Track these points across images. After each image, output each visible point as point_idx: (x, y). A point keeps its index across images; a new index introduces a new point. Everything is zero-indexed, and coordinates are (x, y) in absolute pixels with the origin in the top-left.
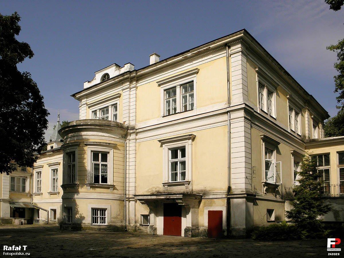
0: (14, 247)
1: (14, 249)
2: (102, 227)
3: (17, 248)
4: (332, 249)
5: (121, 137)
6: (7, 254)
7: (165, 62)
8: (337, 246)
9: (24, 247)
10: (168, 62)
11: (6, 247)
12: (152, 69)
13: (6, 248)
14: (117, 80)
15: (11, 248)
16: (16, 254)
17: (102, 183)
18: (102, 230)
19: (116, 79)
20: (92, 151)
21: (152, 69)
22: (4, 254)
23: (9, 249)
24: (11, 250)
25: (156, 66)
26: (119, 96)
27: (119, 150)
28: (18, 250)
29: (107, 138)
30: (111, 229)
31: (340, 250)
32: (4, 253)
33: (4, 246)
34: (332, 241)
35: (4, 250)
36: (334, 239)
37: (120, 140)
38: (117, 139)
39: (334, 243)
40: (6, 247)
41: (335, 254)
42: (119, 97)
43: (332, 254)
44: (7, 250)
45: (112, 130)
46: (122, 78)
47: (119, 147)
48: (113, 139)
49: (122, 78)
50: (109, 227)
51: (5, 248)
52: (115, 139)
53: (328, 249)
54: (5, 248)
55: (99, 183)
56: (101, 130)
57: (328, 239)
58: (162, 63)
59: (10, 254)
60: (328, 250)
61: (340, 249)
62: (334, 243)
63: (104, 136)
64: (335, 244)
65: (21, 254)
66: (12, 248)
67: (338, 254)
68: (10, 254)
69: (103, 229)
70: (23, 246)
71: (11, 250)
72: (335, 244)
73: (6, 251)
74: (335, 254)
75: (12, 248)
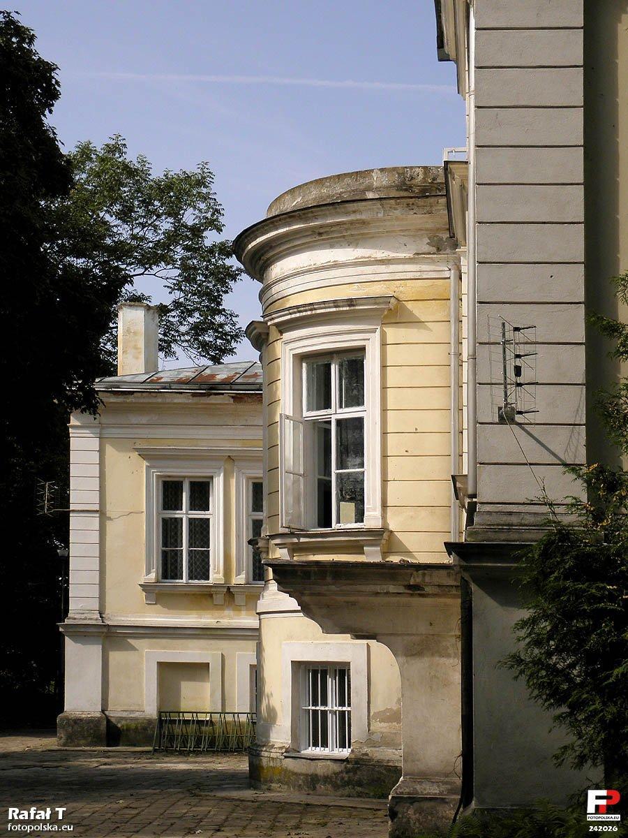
0: (35, 812)
2: (320, 769)
3: (42, 813)
4: (598, 816)
5: (426, 248)
8: (610, 809)
9: (58, 811)
11: (14, 811)
15: (26, 813)
16: (40, 828)
18: (321, 787)
22: (11, 828)
24: (27, 818)
27: (415, 322)
28: (43, 818)
29: (351, 271)
30: (360, 784)
31: (619, 820)
32: (9, 826)
33: (11, 810)
34: (598, 798)
35: (10, 818)
36: (603, 793)
37: (424, 267)
38: (400, 267)
39: (603, 802)
40: (14, 811)
43: (599, 828)
44: (16, 818)
45: (363, 222)
47: (416, 309)
48: (382, 268)
50: (354, 771)
52: (393, 268)
54: (13, 813)
56: (320, 234)
59: (24, 828)
60: (590, 820)
61: (619, 816)
62: (603, 802)
63: (336, 265)
64: (605, 804)
68: (24, 828)
69: (326, 779)
70: (57, 809)
71: (27, 818)
72: (605, 804)
73: (14, 821)
74: (605, 829)
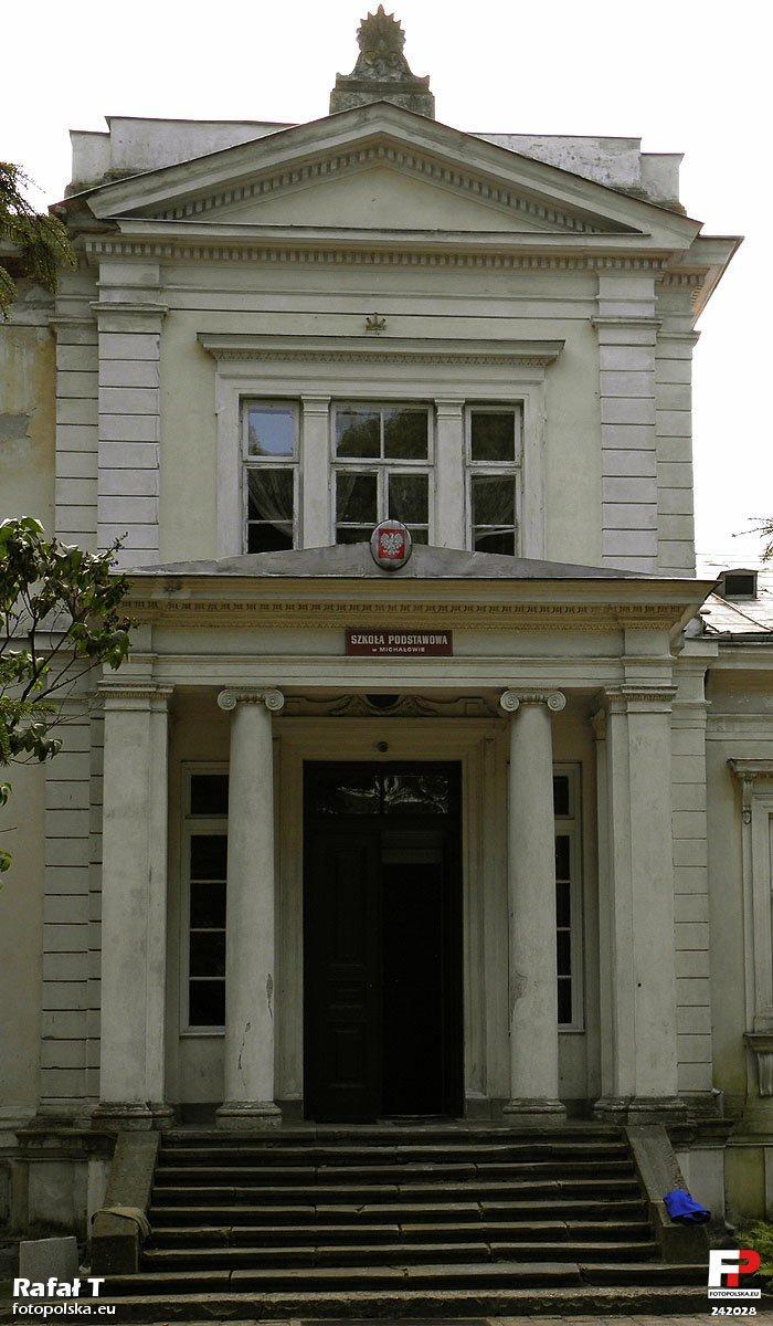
0: (55, 1285)
4: (726, 1291)
8: (744, 1281)
9: (92, 1284)
11: (22, 1284)
13: (24, 1289)
15: (41, 1287)
17: (394, 479)
22: (17, 1310)
23: (33, 1293)
24: (42, 1294)
26: (545, 357)
28: (68, 1294)
31: (759, 1297)
32: (15, 1307)
34: (725, 1262)
35: (16, 1294)
36: (734, 1254)
39: (734, 1269)
40: (22, 1284)
42: (549, 363)
43: (727, 1311)
44: (25, 1294)
51: (21, 1286)
55: (374, 520)
57: (711, 1252)
59: (39, 1310)
62: (734, 1269)
65: (82, 1310)
66: (46, 1289)
68: (39, 1310)
70: (90, 1280)
71: (42, 1294)
75: (46, 1289)
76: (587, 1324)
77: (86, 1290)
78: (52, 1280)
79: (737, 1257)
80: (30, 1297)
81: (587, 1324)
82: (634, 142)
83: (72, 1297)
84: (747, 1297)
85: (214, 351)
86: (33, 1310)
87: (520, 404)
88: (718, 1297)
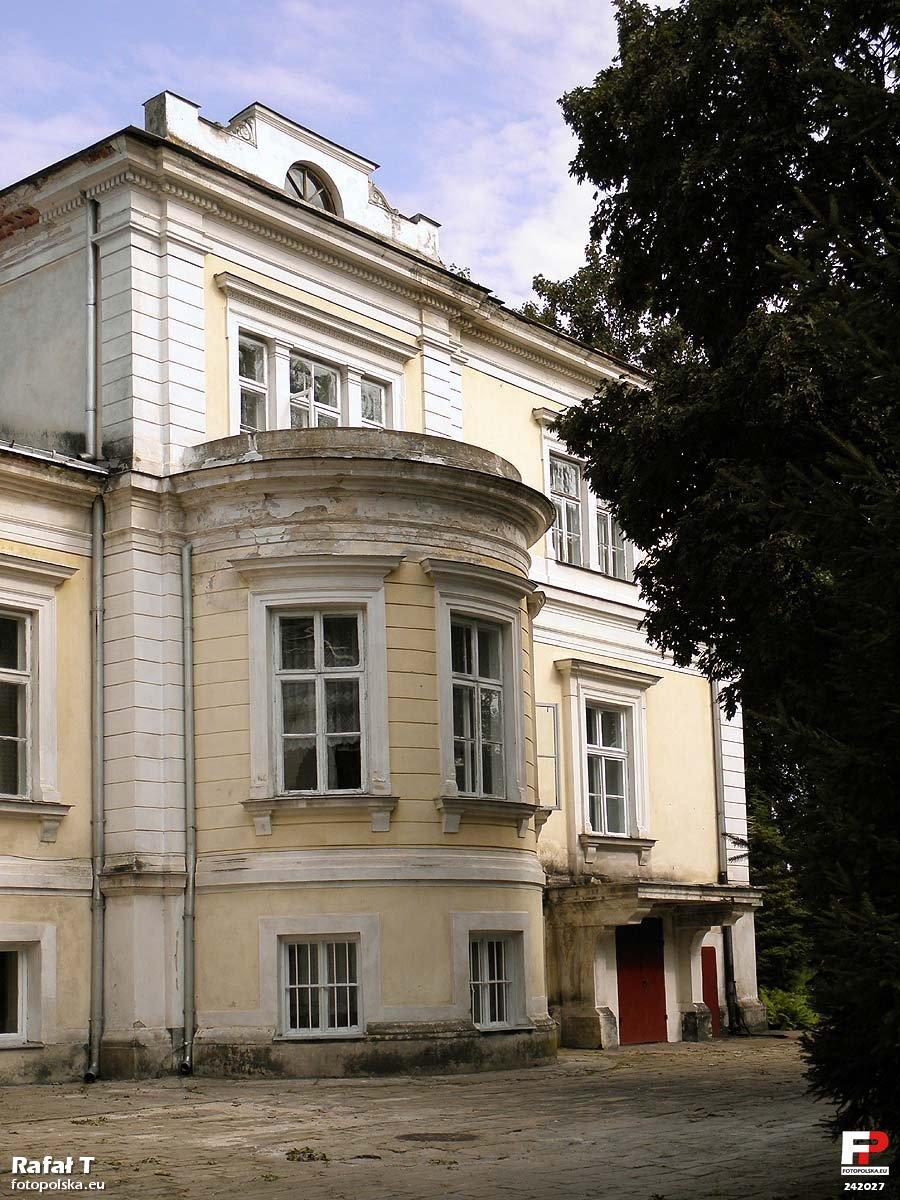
0: (50, 1162)
1: (50, 1170)
4: (857, 1168)
6: (26, 1185)
7: (582, 357)
9: (83, 1162)
10: (589, 364)
11: (20, 1162)
12: (540, 342)
13: (22, 1166)
14: (424, 281)
15: (37, 1164)
16: (57, 1185)
19: (421, 275)
20: (271, 610)
21: (540, 342)
22: (16, 1185)
23: (30, 1170)
24: (38, 1171)
25: (556, 344)
28: (62, 1171)
31: (887, 1174)
32: (13, 1183)
33: (15, 1160)
34: (857, 1142)
35: (15, 1171)
36: (865, 1135)
39: (865, 1149)
40: (20, 1162)
41: (868, 1187)
43: (858, 1186)
44: (23, 1171)
46: (450, 293)
49: (450, 293)
53: (843, 1168)
57: (844, 1133)
58: (578, 350)
59: (35, 1185)
61: (888, 1168)
62: (865, 1149)
66: (42, 1167)
67: (879, 1186)
68: (35, 1185)
70: (81, 1159)
73: (21, 1177)
74: (868, 1187)
75: (42, 1167)
76: (12, 1198)
77: (78, 1165)
78: (47, 1158)
79: (868, 1138)
80: (27, 1174)
81: (12, 1198)
82: (487, 291)
83: (65, 1174)
84: (876, 1174)
85: (225, 287)
86: (30, 1185)
87: (32, 613)
88: (850, 1174)
